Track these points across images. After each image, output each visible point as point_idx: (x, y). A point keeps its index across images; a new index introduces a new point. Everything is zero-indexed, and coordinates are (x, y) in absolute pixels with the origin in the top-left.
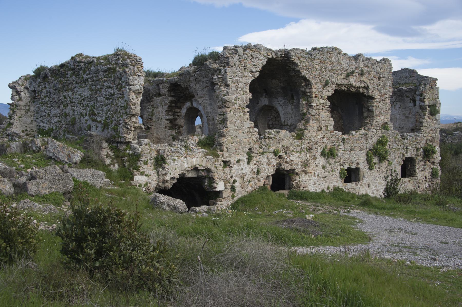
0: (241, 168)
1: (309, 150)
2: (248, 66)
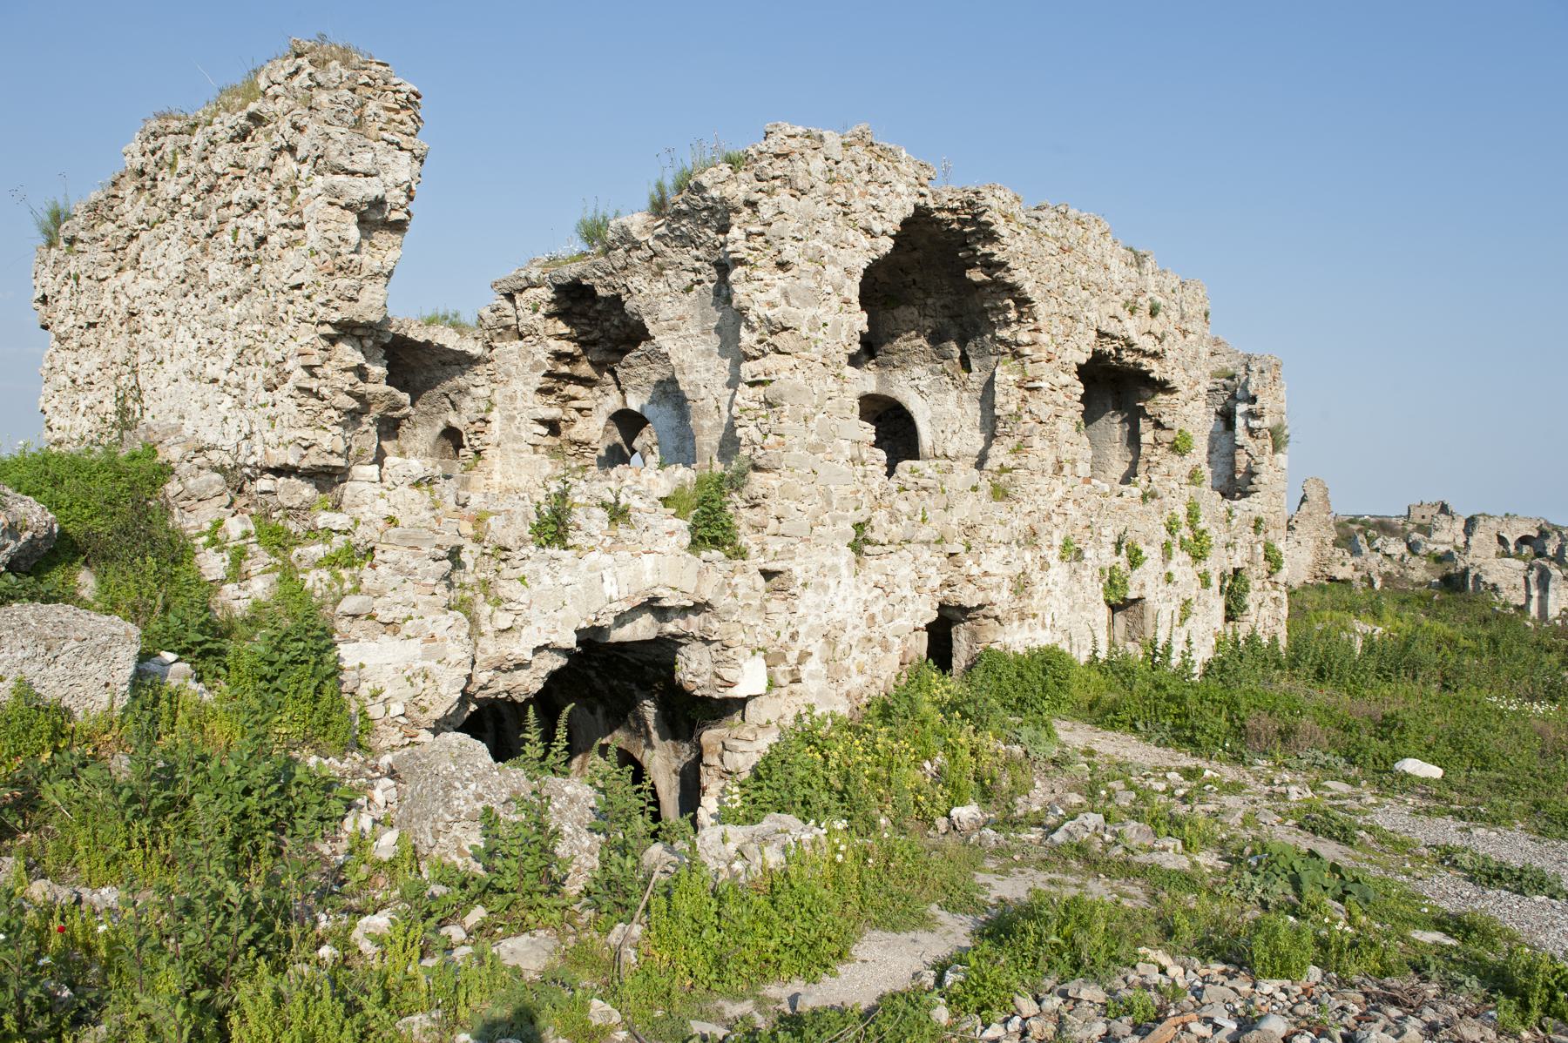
0: (827, 599)
1: (1031, 538)
2: (858, 205)
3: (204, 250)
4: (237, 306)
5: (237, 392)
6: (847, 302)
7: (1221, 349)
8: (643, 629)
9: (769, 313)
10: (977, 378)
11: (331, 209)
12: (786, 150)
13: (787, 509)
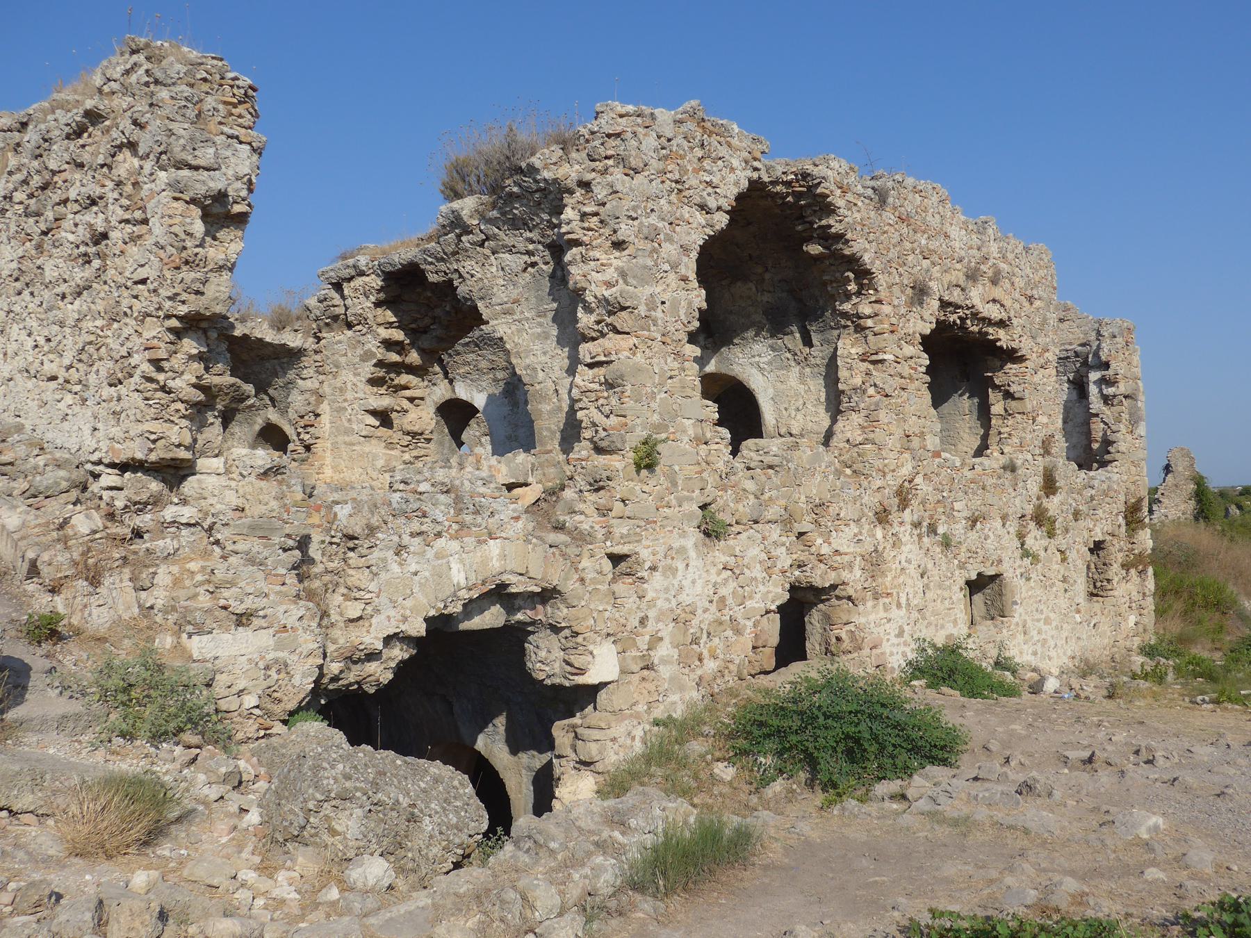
0: (676, 582)
2: (692, 181)
3: (39, 247)
4: (77, 302)
5: (78, 388)
6: (685, 279)
7: (1070, 315)
8: (492, 617)
9: (607, 294)
10: (819, 353)
11: (176, 204)
12: (619, 129)
13: (632, 491)
